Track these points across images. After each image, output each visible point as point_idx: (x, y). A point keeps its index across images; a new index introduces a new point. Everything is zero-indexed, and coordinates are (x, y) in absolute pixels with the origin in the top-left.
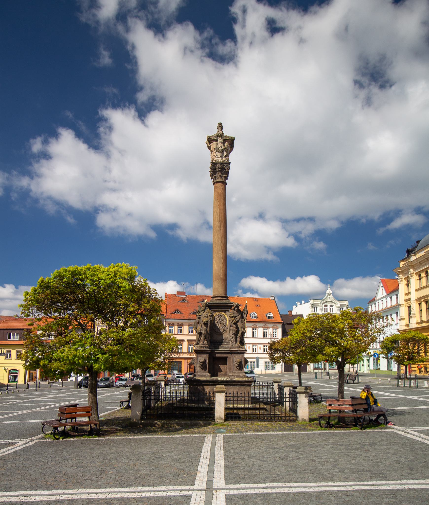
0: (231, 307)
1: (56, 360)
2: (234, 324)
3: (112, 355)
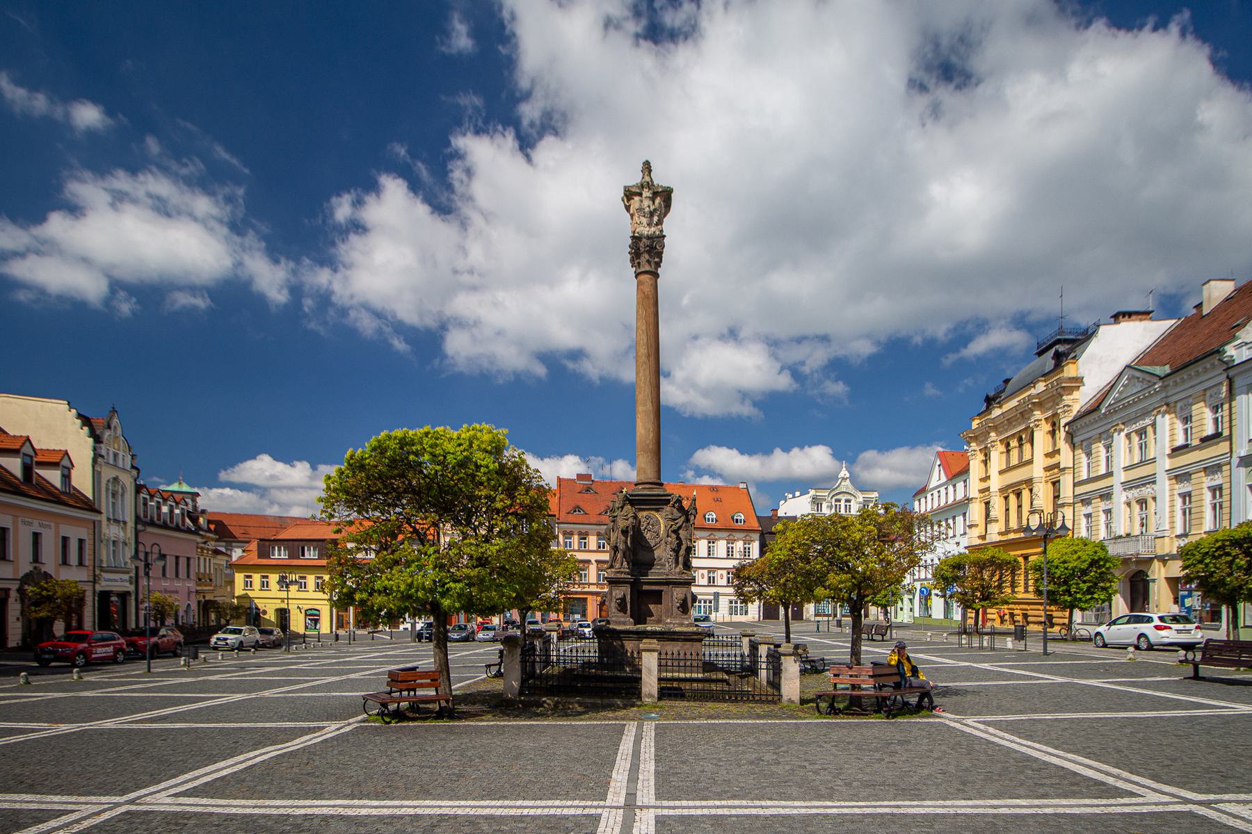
0: (669, 501)
1: (380, 592)
2: (674, 531)
3: (470, 585)
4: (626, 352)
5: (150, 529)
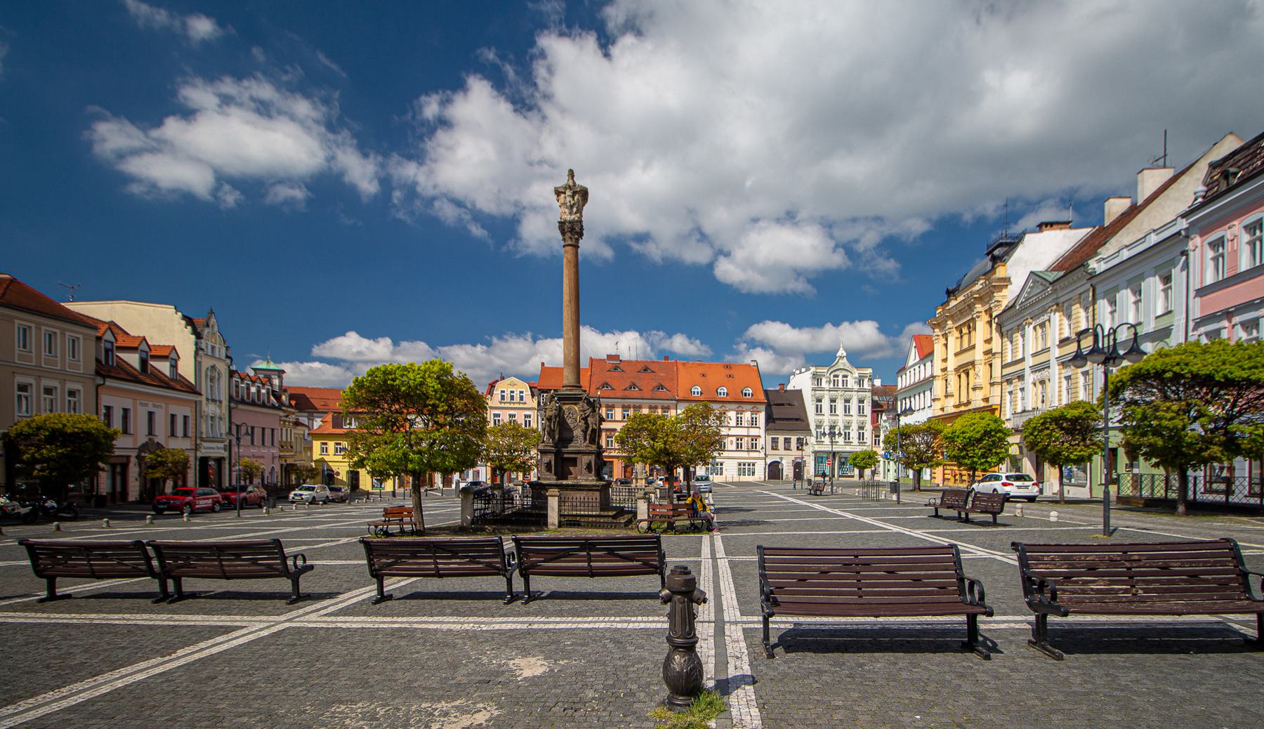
4: (690, 235)
5: (240, 406)
